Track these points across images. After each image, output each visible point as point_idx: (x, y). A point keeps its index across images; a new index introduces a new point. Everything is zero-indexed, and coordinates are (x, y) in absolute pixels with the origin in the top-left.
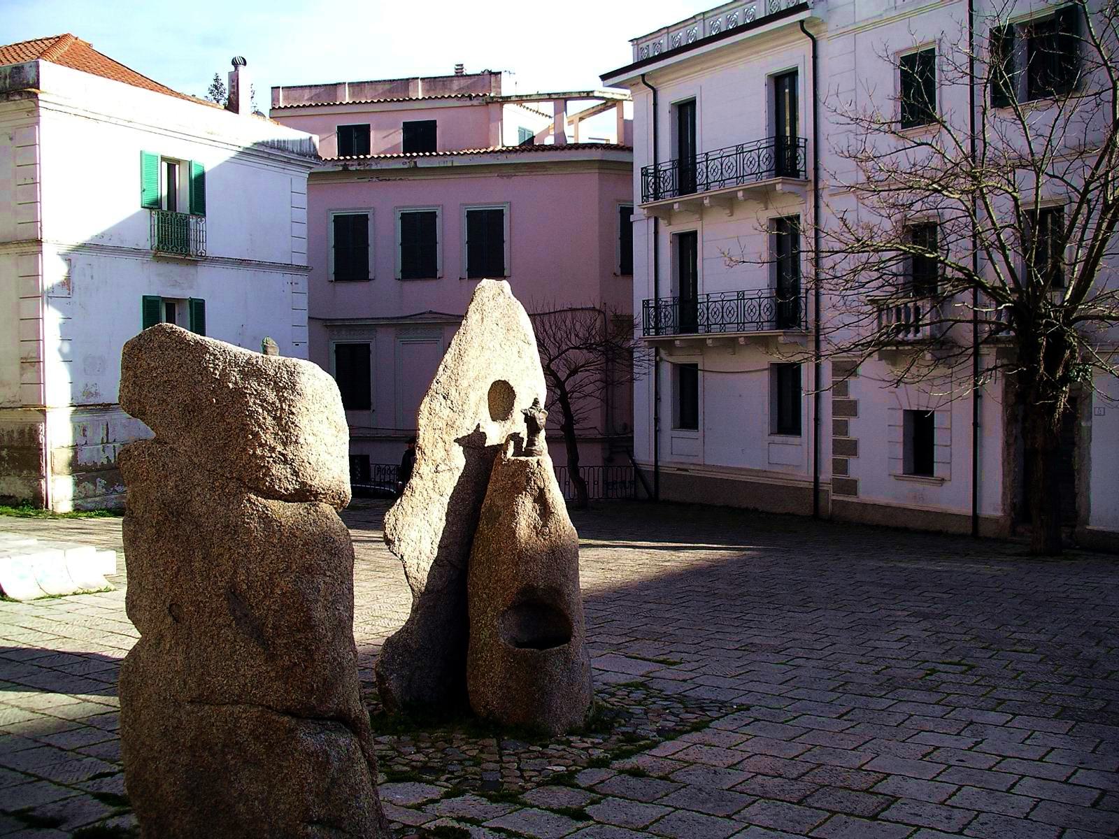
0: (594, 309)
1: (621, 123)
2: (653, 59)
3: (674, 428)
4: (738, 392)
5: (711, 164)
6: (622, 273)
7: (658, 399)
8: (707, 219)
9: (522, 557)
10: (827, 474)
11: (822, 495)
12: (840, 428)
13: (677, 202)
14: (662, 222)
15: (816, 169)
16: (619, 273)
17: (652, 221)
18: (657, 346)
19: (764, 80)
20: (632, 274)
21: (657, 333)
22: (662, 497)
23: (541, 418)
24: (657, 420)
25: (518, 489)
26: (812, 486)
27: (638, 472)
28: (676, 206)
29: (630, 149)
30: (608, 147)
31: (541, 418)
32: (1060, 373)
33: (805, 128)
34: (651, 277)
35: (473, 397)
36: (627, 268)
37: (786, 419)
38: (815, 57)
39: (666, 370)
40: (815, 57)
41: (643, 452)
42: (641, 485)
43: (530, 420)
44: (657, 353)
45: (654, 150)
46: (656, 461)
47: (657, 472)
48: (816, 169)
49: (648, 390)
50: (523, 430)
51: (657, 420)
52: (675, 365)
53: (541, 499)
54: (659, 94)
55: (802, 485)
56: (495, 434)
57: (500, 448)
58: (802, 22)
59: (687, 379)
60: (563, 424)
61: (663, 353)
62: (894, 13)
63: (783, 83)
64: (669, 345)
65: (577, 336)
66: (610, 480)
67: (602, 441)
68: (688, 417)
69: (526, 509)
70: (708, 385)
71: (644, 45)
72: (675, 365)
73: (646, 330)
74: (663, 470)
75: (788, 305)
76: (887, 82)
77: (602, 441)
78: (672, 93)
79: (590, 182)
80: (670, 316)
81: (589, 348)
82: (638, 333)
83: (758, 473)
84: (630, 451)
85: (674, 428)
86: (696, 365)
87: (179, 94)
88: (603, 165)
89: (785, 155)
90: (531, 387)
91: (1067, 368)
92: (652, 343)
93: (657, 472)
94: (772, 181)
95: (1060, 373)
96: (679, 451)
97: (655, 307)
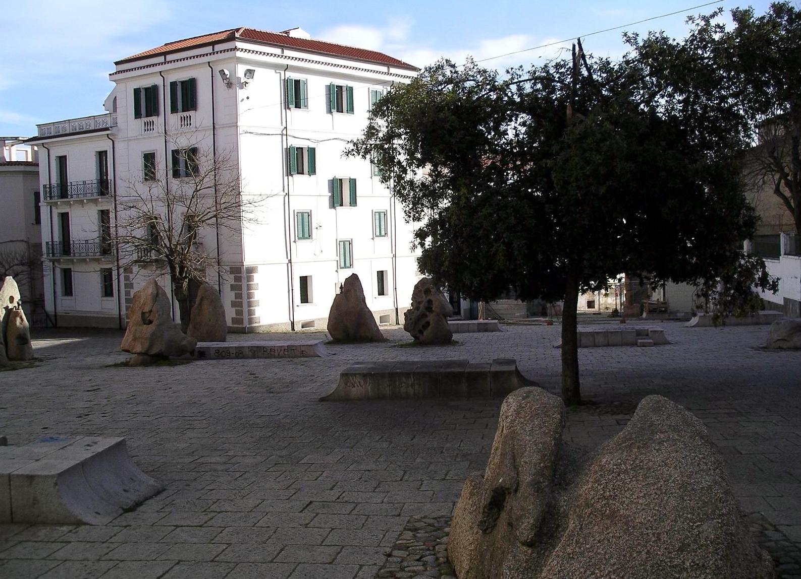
0: (22, 241)
1: (33, 152)
2: (46, 137)
3: (62, 296)
4: (88, 281)
5: (73, 187)
6: (36, 223)
7: (54, 283)
8: (72, 208)
9: (18, 328)
10: (124, 312)
11: (122, 320)
12: (128, 293)
13: (59, 201)
14: (53, 208)
15: (115, 192)
16: (35, 223)
17: (49, 207)
18: (54, 262)
19: (94, 153)
20: (40, 223)
21: (53, 256)
22: (59, 325)
23: (20, 303)
24: (55, 292)
25: (16, 316)
26: (118, 316)
27: (47, 315)
28: (59, 203)
29: (38, 165)
30: (26, 164)
31: (20, 303)
32: (184, 275)
33: (110, 177)
34: (49, 232)
35: (6, 299)
36: (38, 221)
37: (108, 291)
38: (113, 148)
39: (58, 271)
40: (113, 148)
41: (49, 306)
42: (49, 322)
43: (18, 303)
44: (53, 264)
45: (47, 176)
46: (120, 313)
47: (56, 316)
48: (115, 192)
49: (50, 282)
50: (17, 305)
51: (55, 292)
52: (61, 269)
53: (21, 318)
54: (51, 151)
55: (115, 316)
56: (11, 306)
57: (13, 309)
58: (108, 135)
59: (67, 275)
60: (24, 302)
61: (56, 264)
62: (141, 137)
63: (102, 156)
64: (58, 261)
65: (17, 259)
66: (35, 320)
67: (29, 302)
68: (68, 290)
69: (18, 319)
70: (76, 278)
71: (43, 128)
72: (61, 269)
73: (48, 254)
74: (58, 314)
75: (107, 247)
76: (140, 162)
77: (29, 302)
78: (56, 152)
79: (19, 181)
80: (58, 249)
81: (23, 264)
82: (45, 256)
83: (97, 313)
84: (43, 307)
85: (62, 296)
86: (70, 269)
87: (67, 328)
88: (25, 173)
89: (104, 186)
90: (17, 297)
91: (186, 273)
92: (50, 260)
93: (56, 316)
94: (99, 197)
95: (184, 275)
96: (65, 305)
97: (52, 246)
